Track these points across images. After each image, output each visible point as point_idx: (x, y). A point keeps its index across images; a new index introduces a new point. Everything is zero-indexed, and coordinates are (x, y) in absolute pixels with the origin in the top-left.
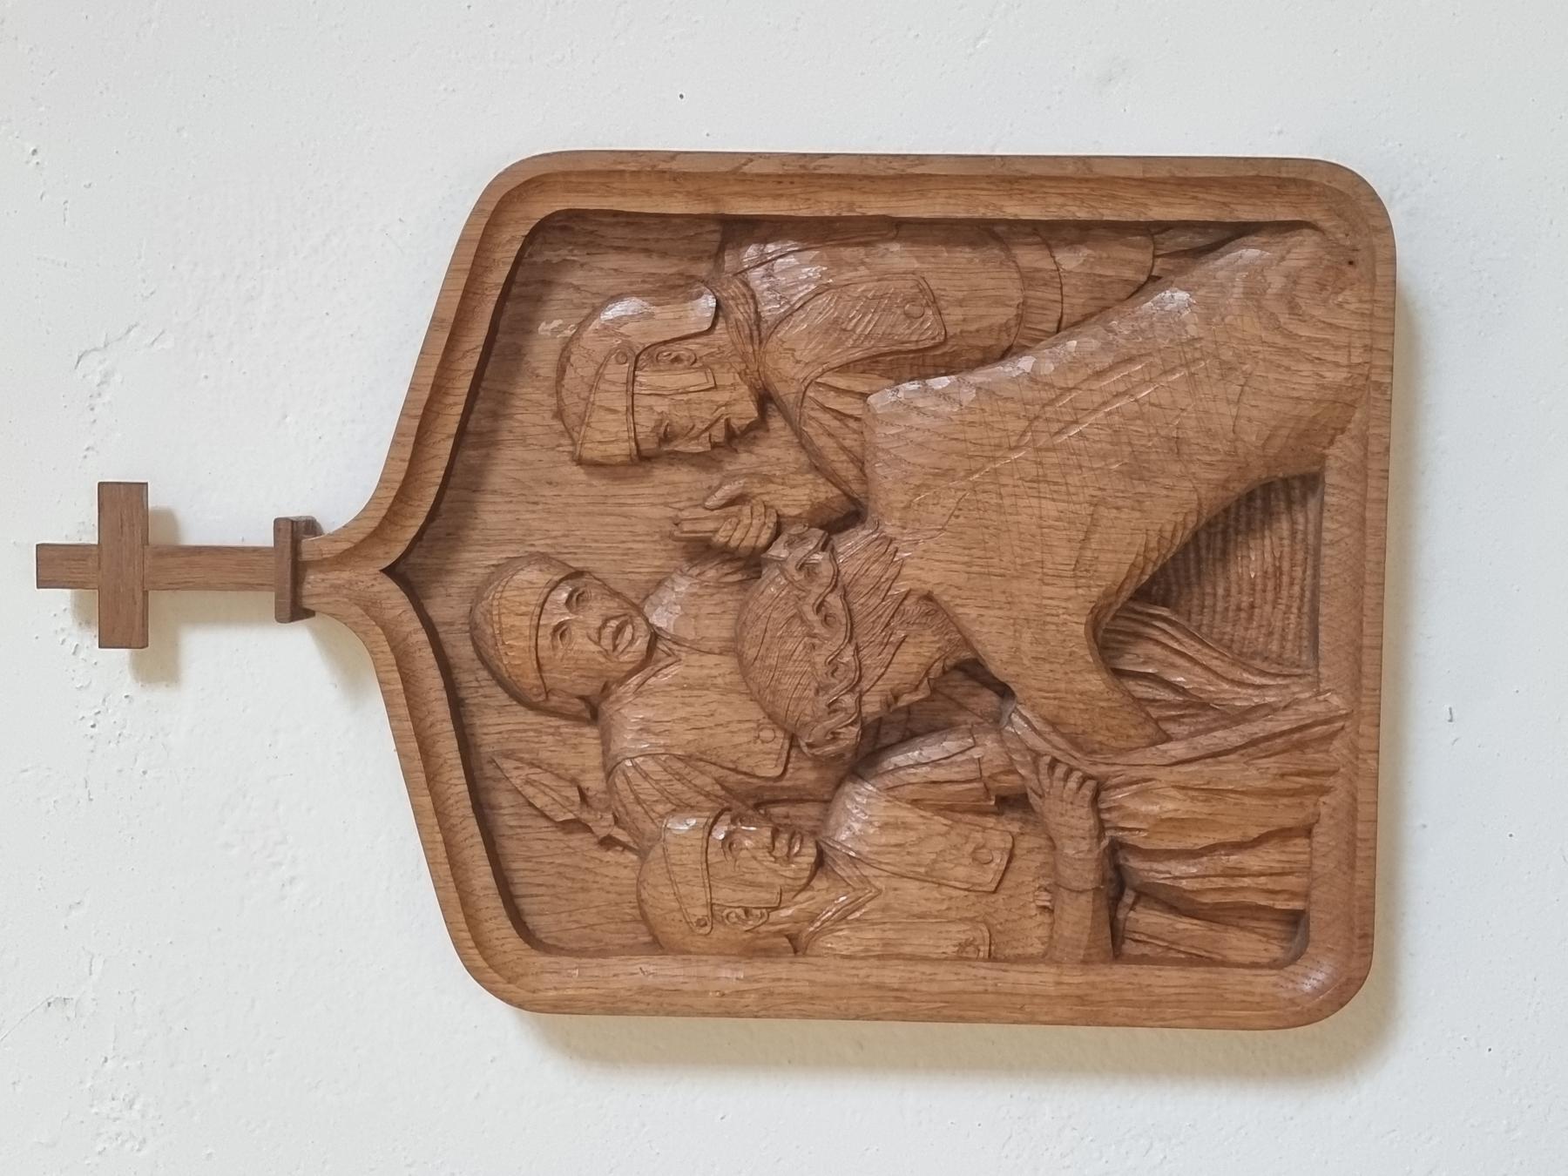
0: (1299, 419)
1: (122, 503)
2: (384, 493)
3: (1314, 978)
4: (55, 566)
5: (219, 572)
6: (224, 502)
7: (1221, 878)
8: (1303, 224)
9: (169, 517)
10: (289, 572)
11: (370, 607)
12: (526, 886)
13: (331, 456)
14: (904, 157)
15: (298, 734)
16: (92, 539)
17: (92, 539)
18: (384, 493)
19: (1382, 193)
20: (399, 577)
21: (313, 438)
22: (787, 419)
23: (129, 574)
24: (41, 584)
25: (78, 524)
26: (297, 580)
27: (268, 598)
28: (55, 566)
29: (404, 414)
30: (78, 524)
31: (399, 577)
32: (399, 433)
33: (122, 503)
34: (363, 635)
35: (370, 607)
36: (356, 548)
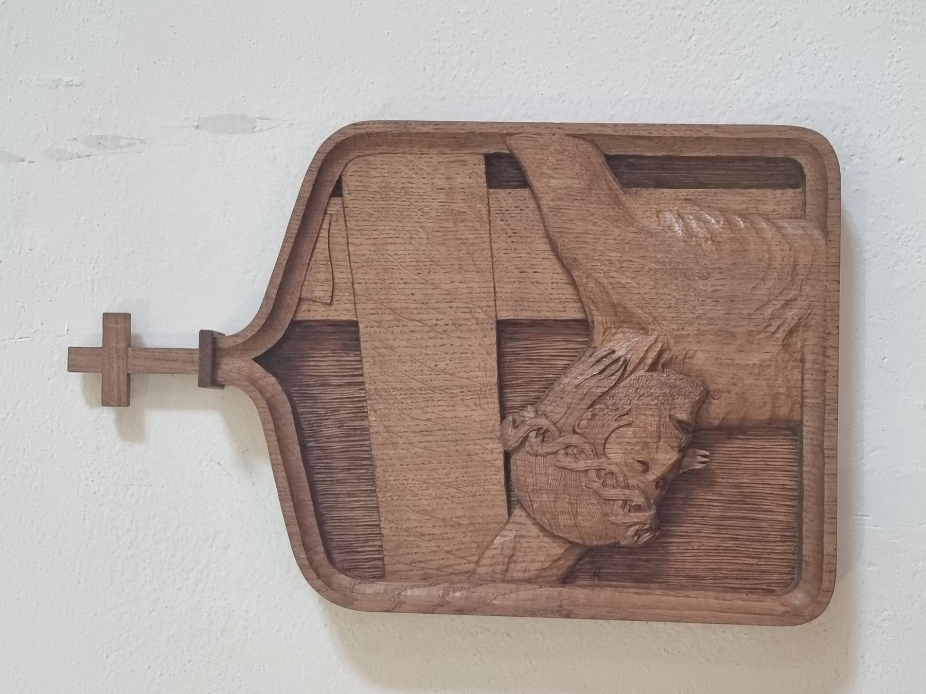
1: (117, 324)
3: (798, 598)
4: (78, 360)
5: (167, 360)
6: (172, 326)
8: (785, 167)
9: (139, 337)
10: (210, 359)
11: (254, 382)
12: (336, 542)
16: (99, 343)
17: (99, 343)
20: (291, 363)
22: (523, 508)
23: (118, 365)
25: (90, 335)
26: (215, 366)
27: (195, 378)
28: (78, 360)
31: (291, 363)
32: (278, 264)
33: (117, 324)
34: (247, 392)
35: (254, 382)
36: (245, 342)
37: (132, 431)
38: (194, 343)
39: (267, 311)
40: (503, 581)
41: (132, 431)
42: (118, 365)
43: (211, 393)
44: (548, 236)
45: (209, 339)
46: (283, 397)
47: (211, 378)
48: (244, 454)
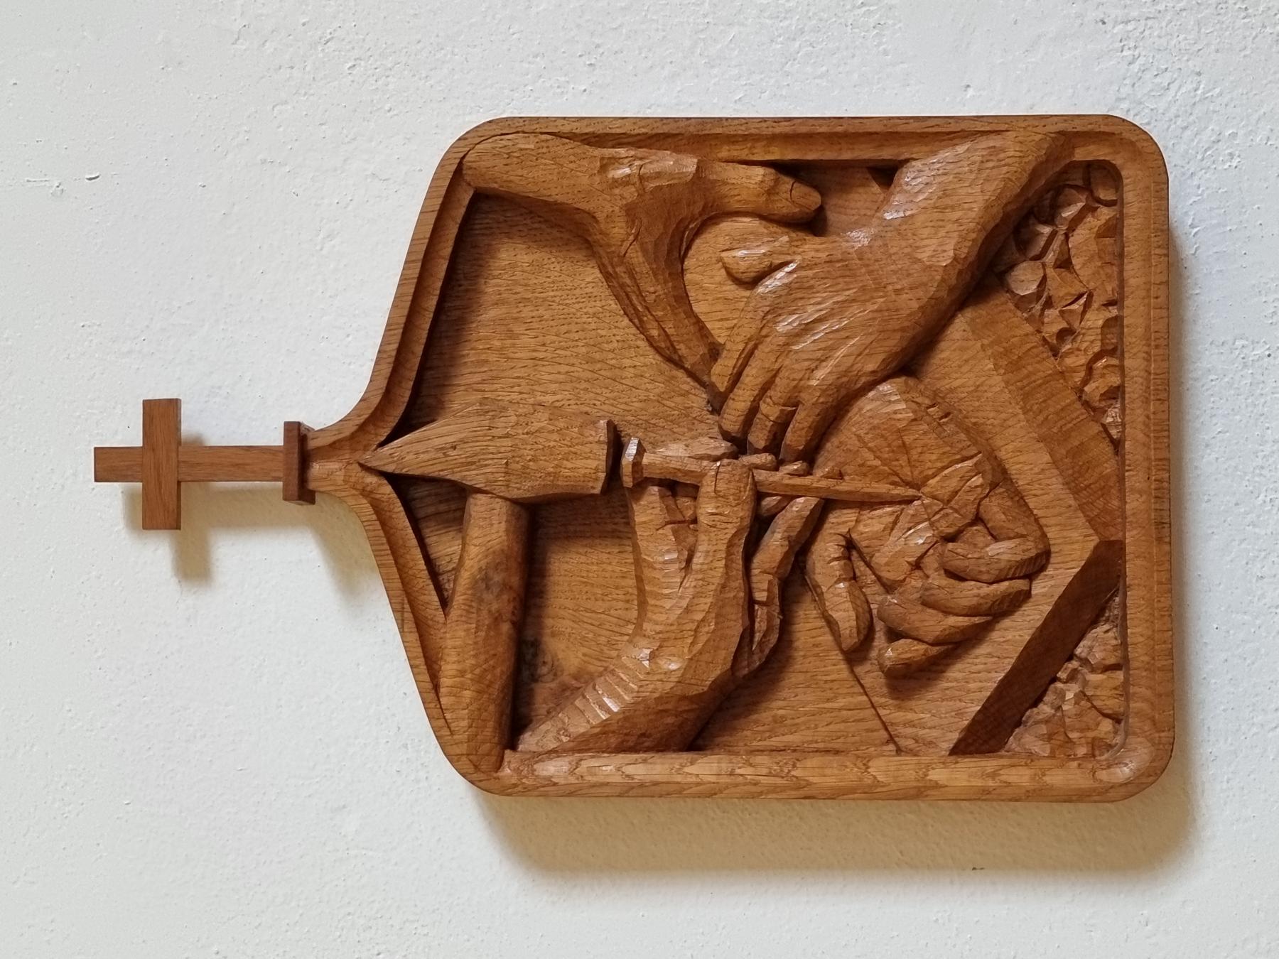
0: (662, 497)
2: (440, 183)
4: (109, 464)
5: (241, 461)
6: (241, 411)
7: (1054, 687)
10: (300, 463)
13: (328, 372)
14: (790, 119)
15: (308, 628)
18: (440, 183)
19: (1172, 160)
20: (387, 476)
21: (315, 358)
23: (168, 477)
24: (96, 480)
25: (130, 434)
28: (109, 464)
29: (401, 285)
30: (130, 434)
31: (387, 476)
32: (403, 280)
33: (161, 415)
37: (194, 568)
38: (276, 438)
39: (383, 383)
40: (691, 374)
41: (194, 568)
42: (168, 477)
43: (305, 509)
44: (727, 161)
45: (297, 433)
46: (398, 508)
47: (304, 493)
48: (347, 581)
